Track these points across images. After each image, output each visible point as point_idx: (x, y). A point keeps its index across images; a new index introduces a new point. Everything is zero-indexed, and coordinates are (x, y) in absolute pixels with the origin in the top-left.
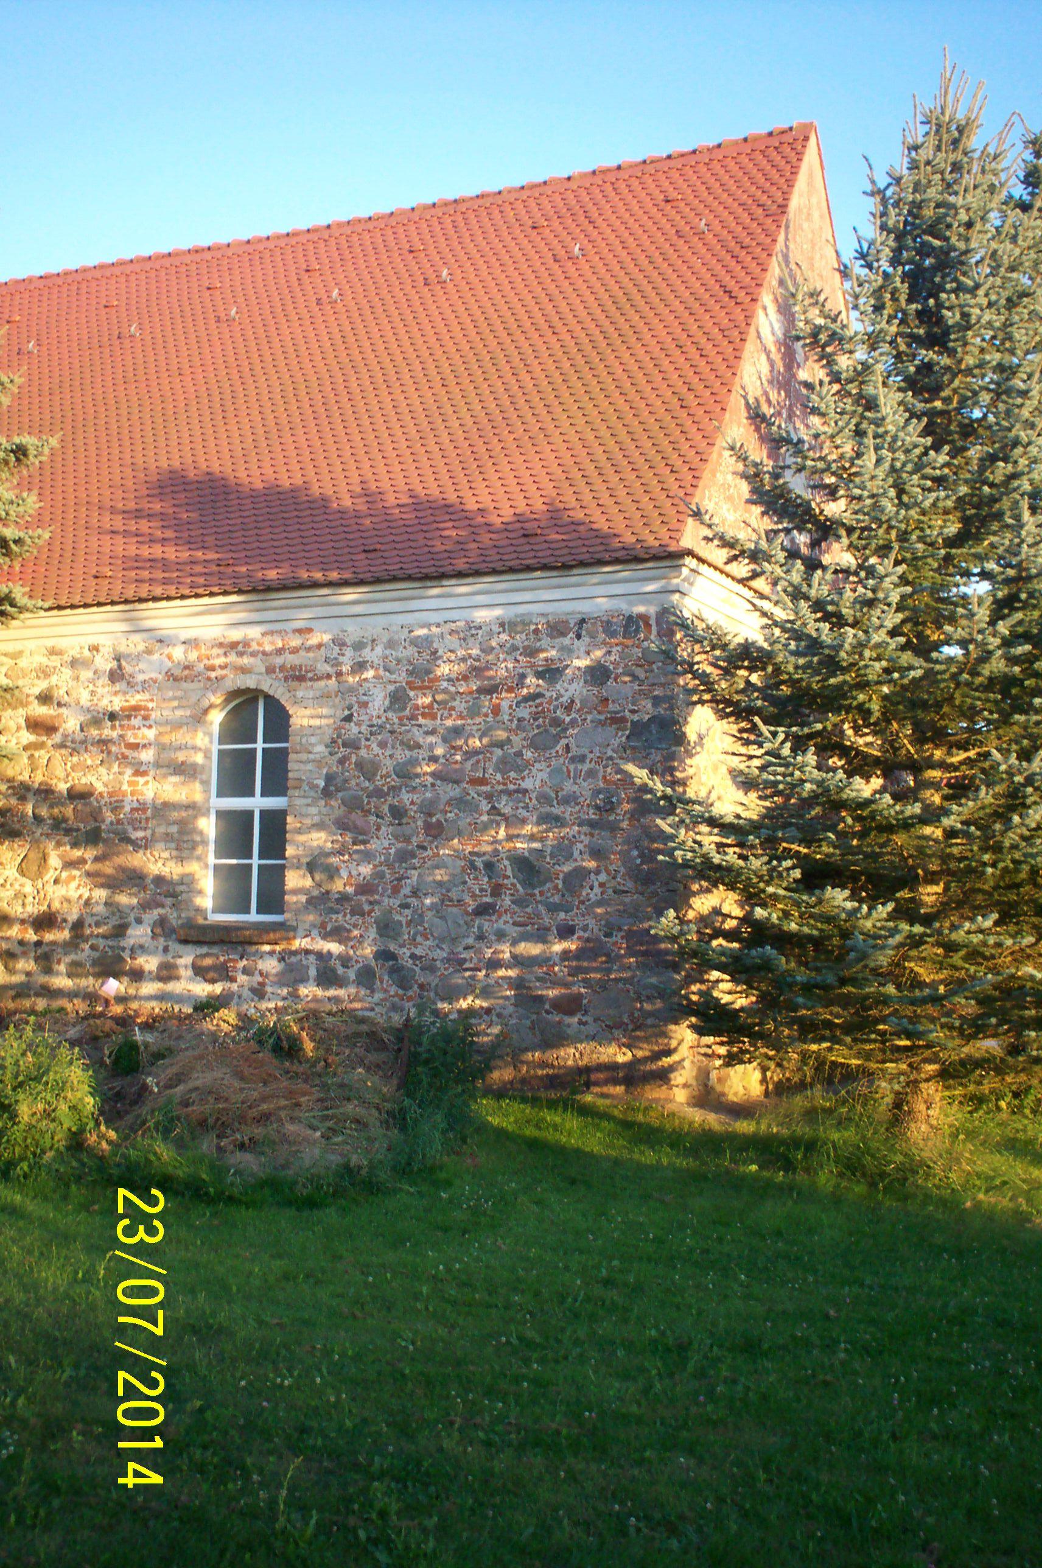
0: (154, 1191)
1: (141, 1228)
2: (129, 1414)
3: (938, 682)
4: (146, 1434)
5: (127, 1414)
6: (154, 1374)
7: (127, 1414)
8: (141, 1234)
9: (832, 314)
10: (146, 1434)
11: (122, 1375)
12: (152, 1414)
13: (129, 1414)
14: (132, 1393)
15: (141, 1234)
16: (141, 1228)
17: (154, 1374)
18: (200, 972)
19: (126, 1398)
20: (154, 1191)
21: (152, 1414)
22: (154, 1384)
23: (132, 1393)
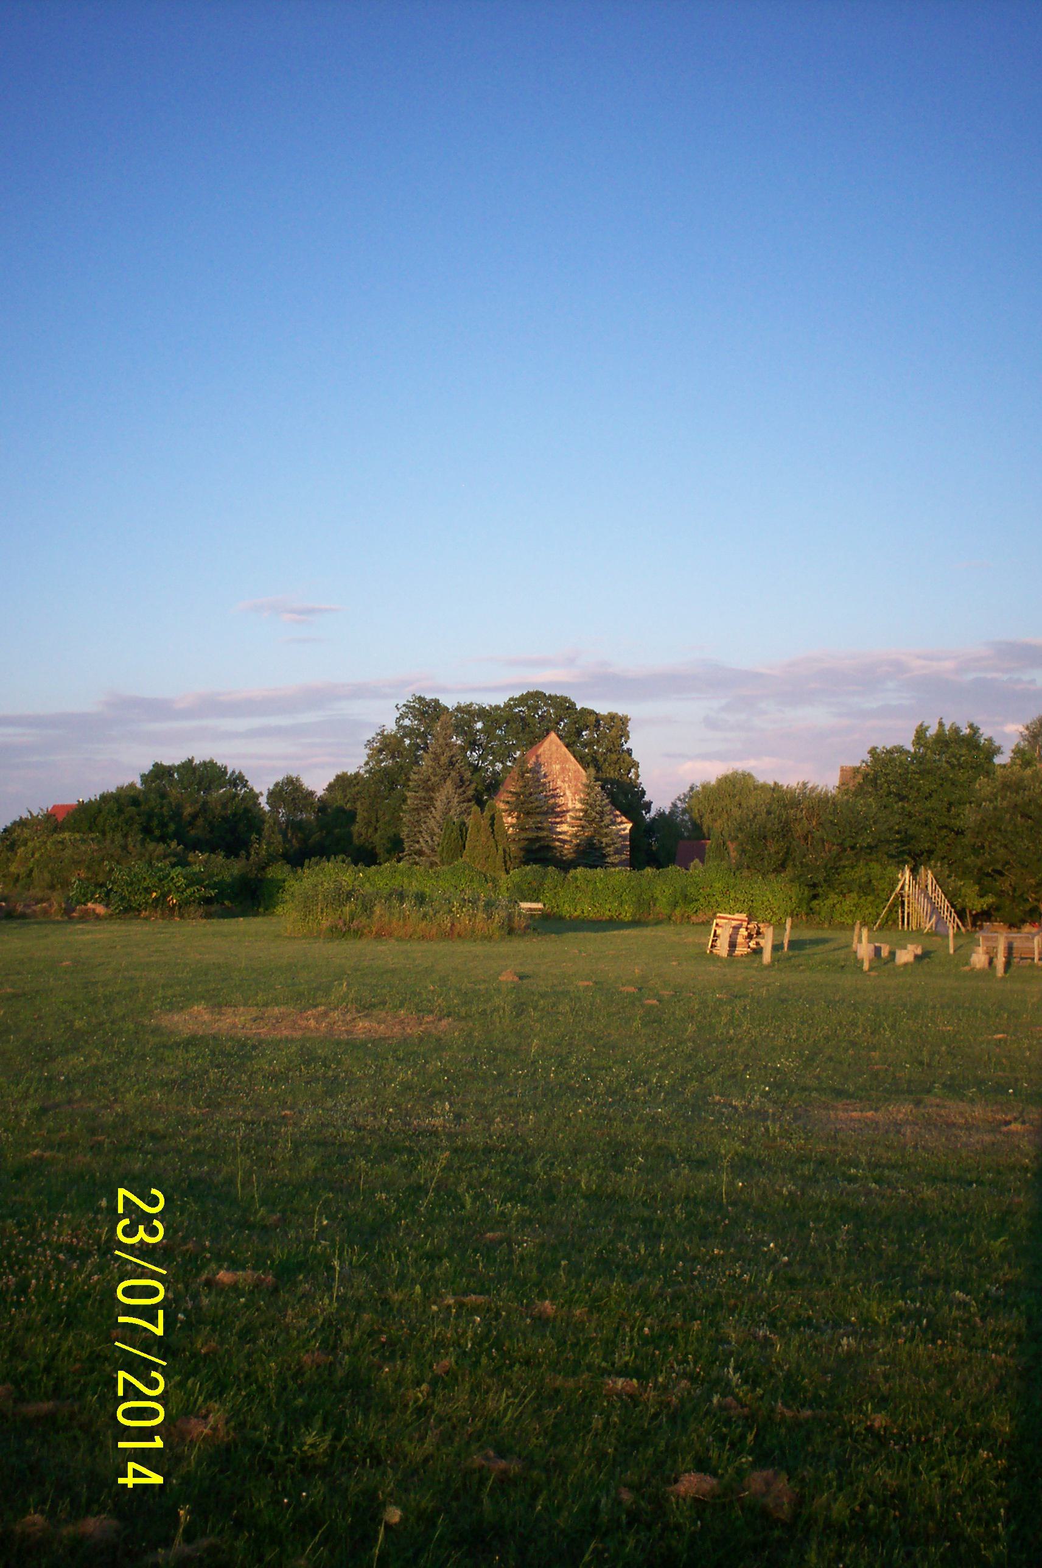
1: (141, 1228)
2: (129, 1414)
4: (147, 1434)
6: (154, 1374)
8: (142, 1234)
10: (147, 1434)
13: (129, 1414)
14: (132, 1393)
15: (142, 1234)
16: (141, 1228)
17: (154, 1374)
22: (153, 1384)
23: (132, 1393)
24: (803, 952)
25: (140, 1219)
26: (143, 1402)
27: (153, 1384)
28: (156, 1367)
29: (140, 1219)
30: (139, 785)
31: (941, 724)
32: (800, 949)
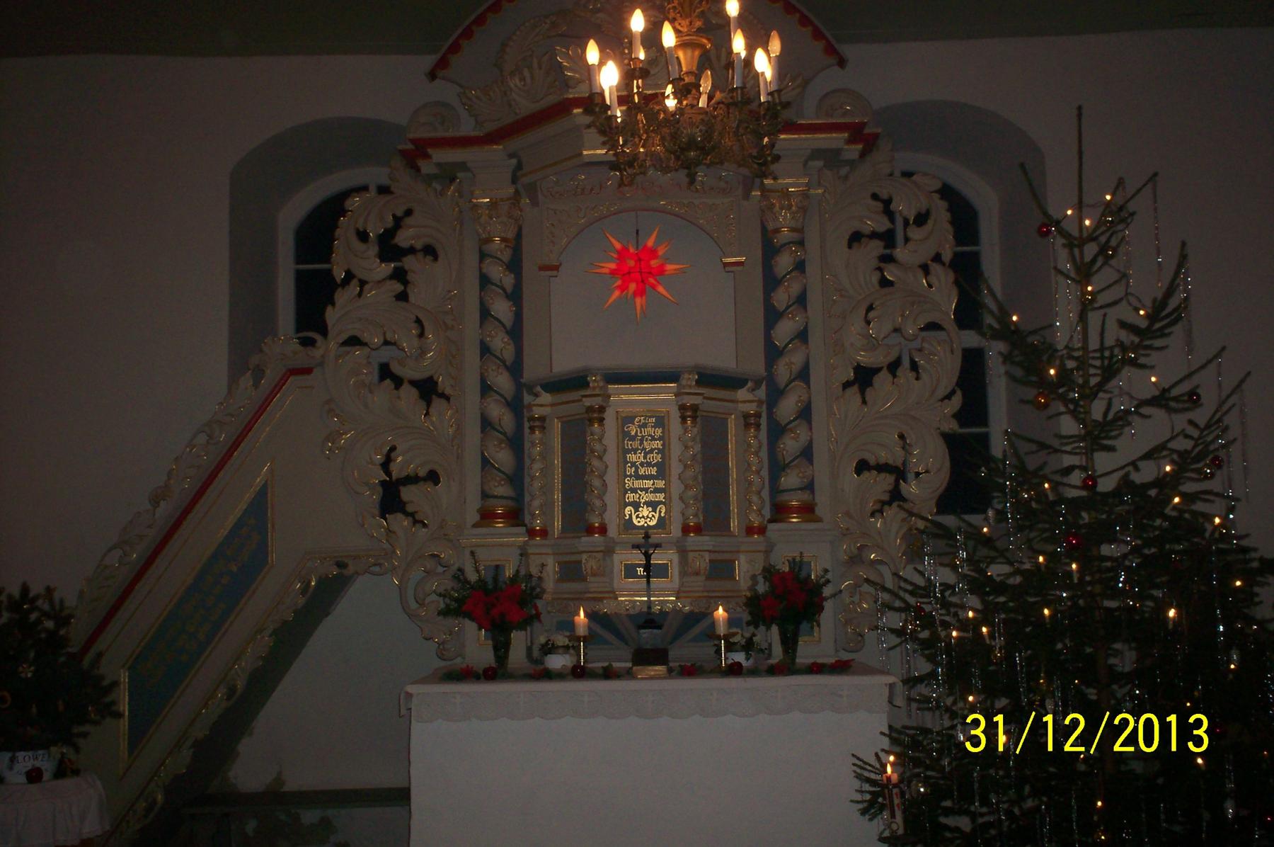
0: (1067, 722)
1: (1195, 732)
2: (1149, 742)
3: (1101, 368)
4: (1165, 728)
5: (1149, 744)
6: (1116, 722)
7: (1149, 744)
8: (978, 732)
9: (388, 381)
10: (1165, 728)
11: (1117, 748)
12: (1149, 723)
13: (1149, 742)
14: (1132, 739)
15: (978, 732)
16: (1195, 732)
17: (1116, 722)
18: (1121, 687)
19: (1136, 744)
20: (1067, 722)
21: (1149, 723)
22: (1125, 723)
23: (1132, 739)
24: (812, 661)
25: (1063, 733)
26: (1139, 732)
27: (1125, 723)
28: (1112, 718)
29: (1063, 733)
30: (624, 108)
31: (882, 733)
32: (814, 664)
